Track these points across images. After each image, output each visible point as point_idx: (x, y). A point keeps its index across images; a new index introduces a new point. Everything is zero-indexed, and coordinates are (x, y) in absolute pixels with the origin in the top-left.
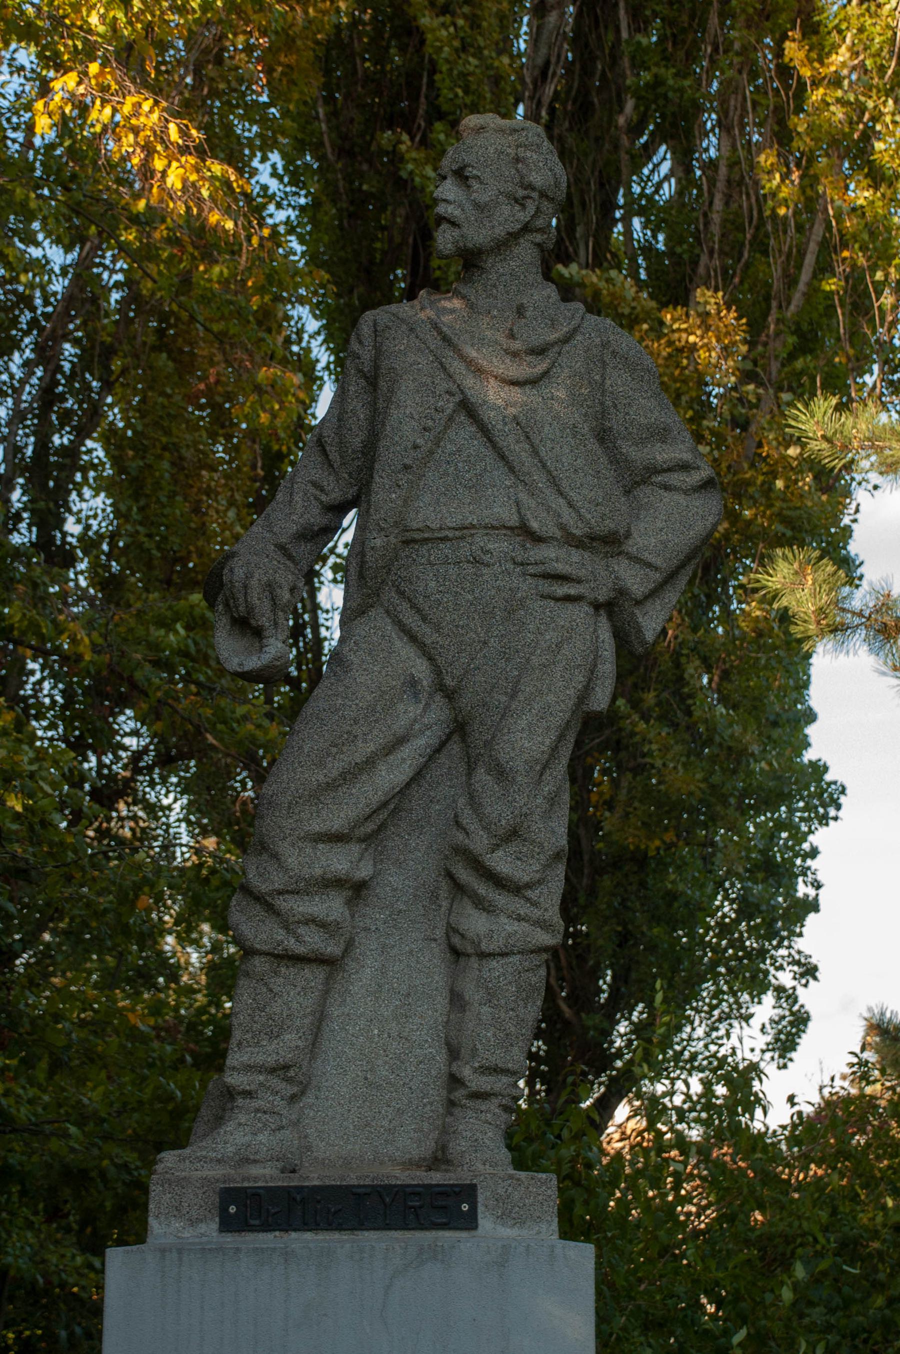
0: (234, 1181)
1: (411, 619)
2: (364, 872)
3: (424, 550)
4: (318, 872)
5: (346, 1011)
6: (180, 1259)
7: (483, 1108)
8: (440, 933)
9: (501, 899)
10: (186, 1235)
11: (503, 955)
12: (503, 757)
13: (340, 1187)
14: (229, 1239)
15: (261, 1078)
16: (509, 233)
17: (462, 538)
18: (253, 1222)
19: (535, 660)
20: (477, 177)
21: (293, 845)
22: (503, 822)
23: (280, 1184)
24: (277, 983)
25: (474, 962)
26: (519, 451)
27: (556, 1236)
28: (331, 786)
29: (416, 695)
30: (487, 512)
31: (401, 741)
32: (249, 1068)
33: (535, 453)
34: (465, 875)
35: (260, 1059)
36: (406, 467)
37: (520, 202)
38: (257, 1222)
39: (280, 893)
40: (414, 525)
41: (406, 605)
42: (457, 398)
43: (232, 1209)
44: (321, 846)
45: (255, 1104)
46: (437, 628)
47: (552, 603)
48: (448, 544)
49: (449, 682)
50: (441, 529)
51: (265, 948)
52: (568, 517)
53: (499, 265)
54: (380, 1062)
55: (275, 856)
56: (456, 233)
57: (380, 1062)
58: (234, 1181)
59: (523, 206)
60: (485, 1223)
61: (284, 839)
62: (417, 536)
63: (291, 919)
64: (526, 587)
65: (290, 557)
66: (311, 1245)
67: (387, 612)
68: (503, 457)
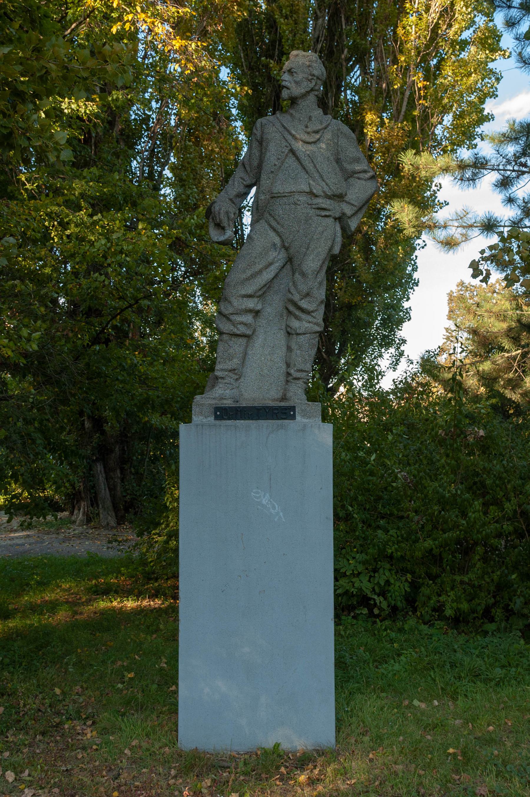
1: (274, 224)
2: (259, 307)
3: (278, 200)
4: (244, 307)
8: (283, 327)
14: (218, 422)
17: (291, 196)
20: (295, 72)
25: (295, 336)
26: (310, 167)
28: (248, 279)
29: (275, 249)
31: (271, 264)
32: (222, 370)
33: (315, 166)
34: (292, 308)
35: (226, 367)
36: (272, 172)
37: (310, 81)
39: (232, 314)
41: (272, 219)
46: (283, 226)
49: (287, 245)
51: (227, 332)
52: (326, 189)
55: (230, 302)
56: (289, 91)
60: (298, 418)
62: (276, 195)
64: (312, 212)
65: (234, 203)
68: (304, 168)
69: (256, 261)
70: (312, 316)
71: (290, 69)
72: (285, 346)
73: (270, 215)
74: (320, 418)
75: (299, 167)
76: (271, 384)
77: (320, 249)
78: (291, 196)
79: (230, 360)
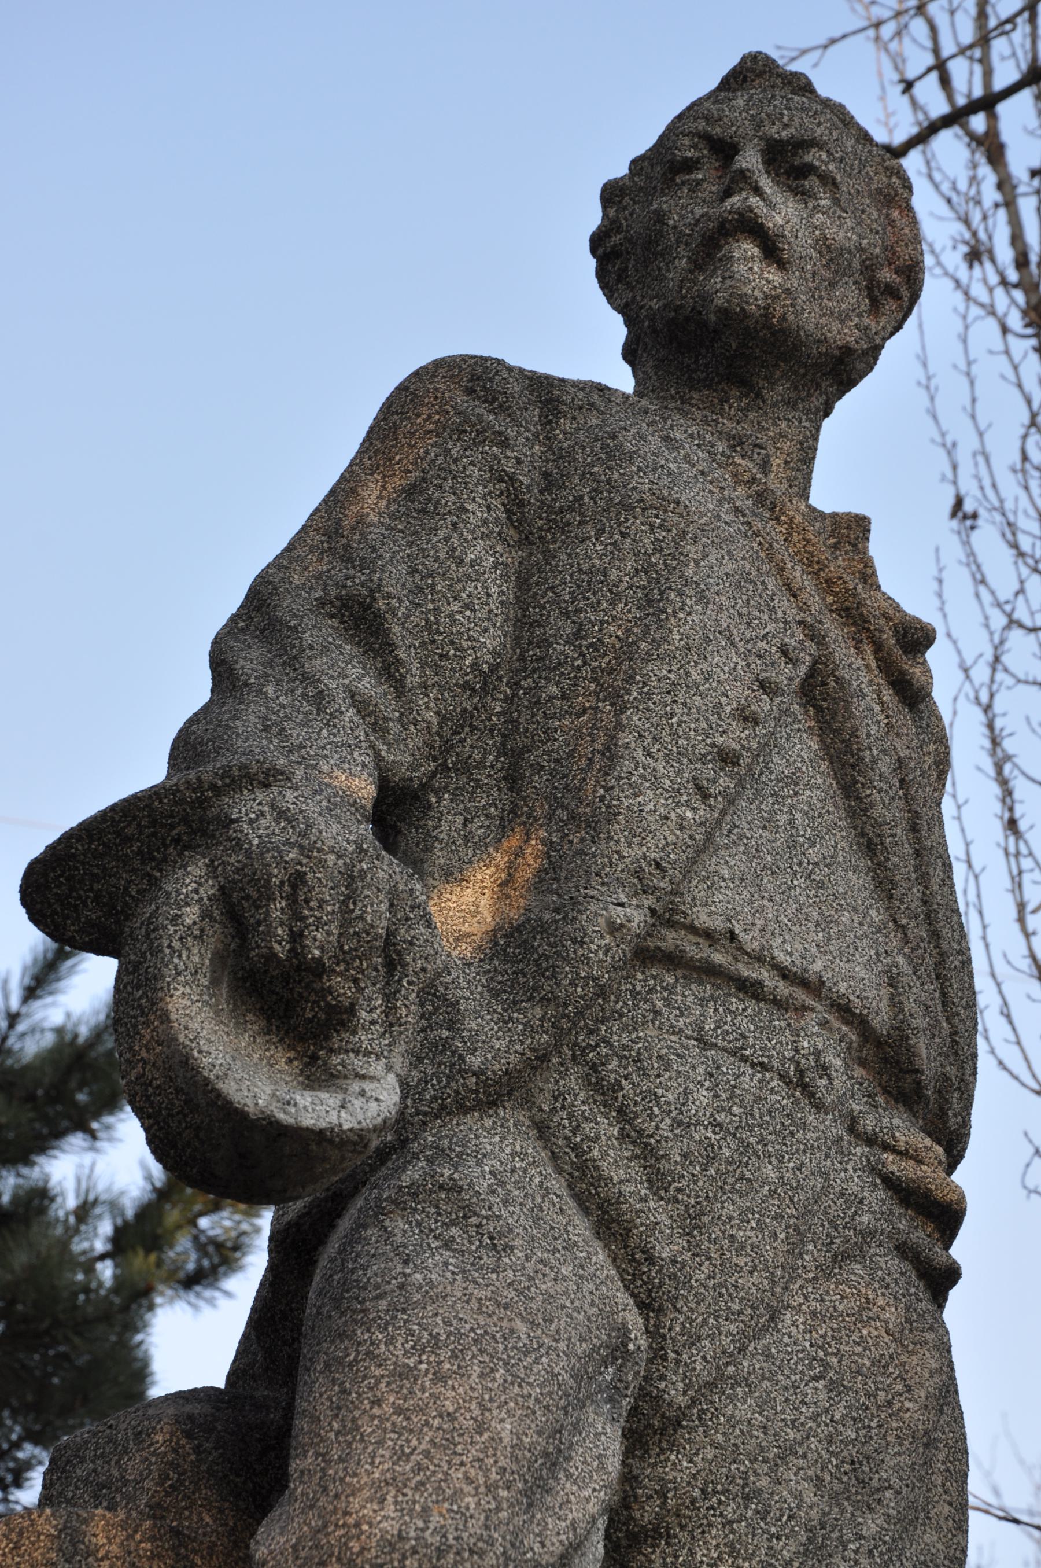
1: (620, 1170)
3: (689, 994)
17: (779, 1004)
20: (828, 181)
40: (702, 918)
41: (608, 1128)
48: (752, 1006)
50: (758, 958)
62: (694, 949)
78: (779, 1004)
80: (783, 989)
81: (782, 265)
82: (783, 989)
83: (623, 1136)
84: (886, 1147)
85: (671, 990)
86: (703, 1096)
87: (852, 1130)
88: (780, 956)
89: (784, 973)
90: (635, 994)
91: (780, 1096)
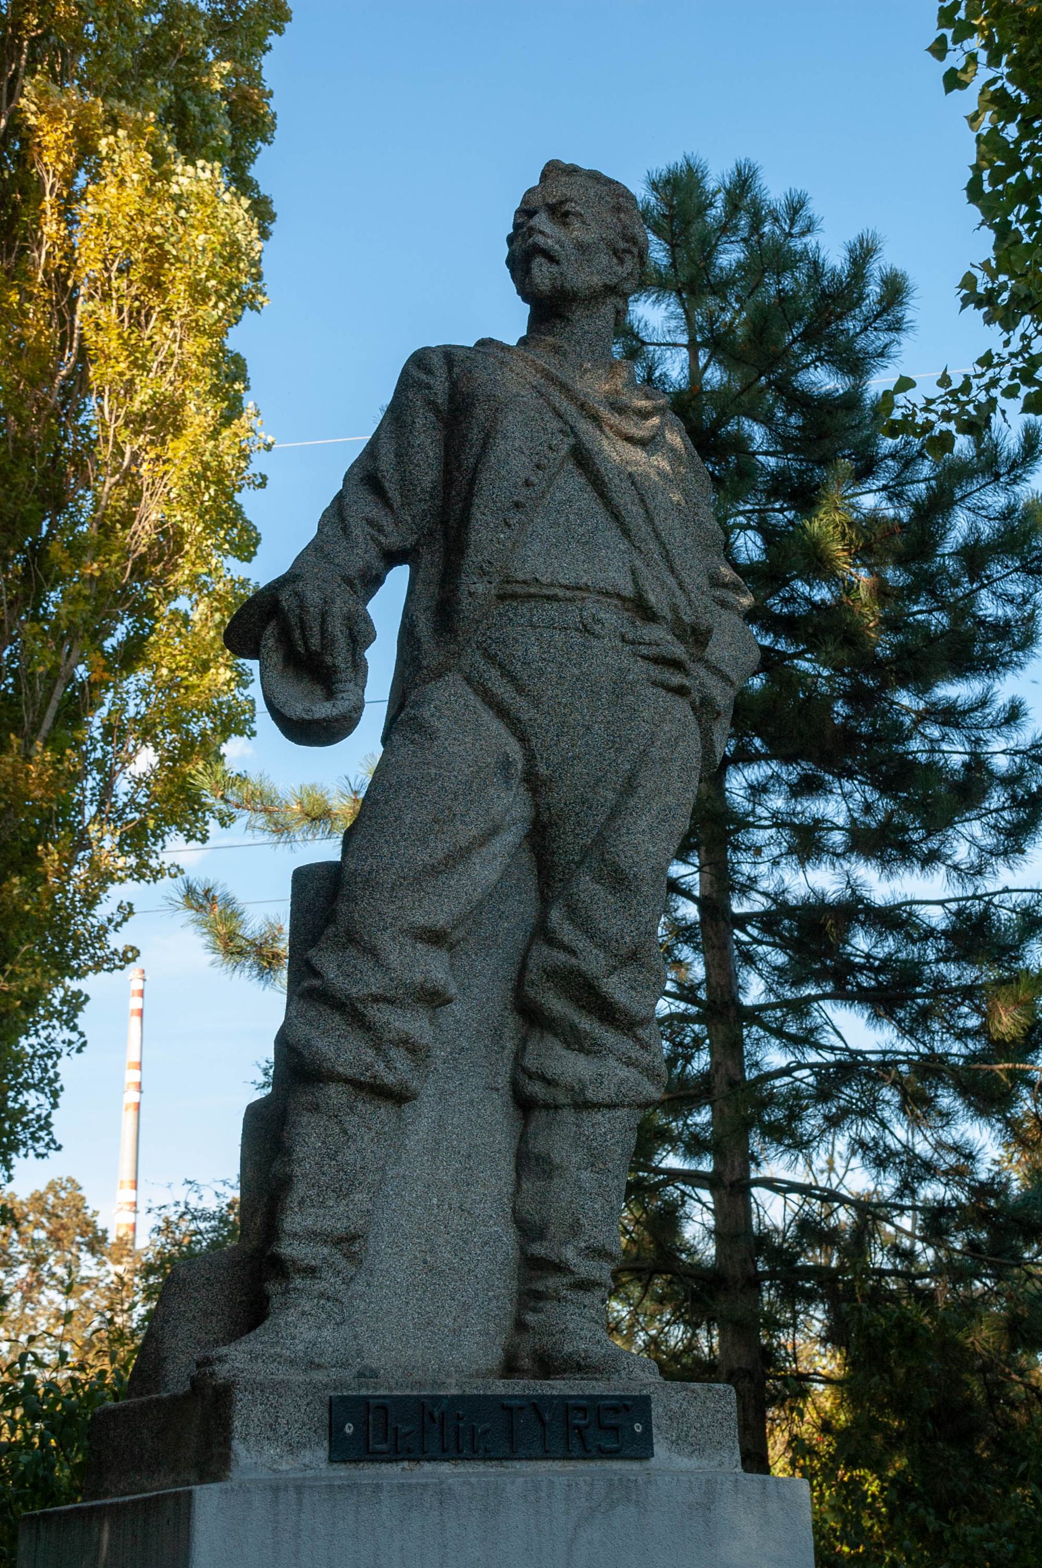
0: (348, 1387)
1: (502, 689)
3: (524, 609)
4: (419, 978)
5: (402, 1171)
6: (300, 1502)
7: (587, 1302)
8: (503, 1081)
9: (609, 1037)
10: (284, 1467)
11: (612, 1106)
12: (624, 863)
13: (485, 1397)
14: (343, 1472)
15: (326, 1251)
16: (605, 286)
17: (571, 600)
18: (379, 1447)
19: (655, 753)
21: (394, 939)
22: (628, 939)
23: (408, 1392)
24: (351, 1121)
25: (568, 1116)
26: (633, 511)
27: (739, 1469)
28: (434, 871)
29: (507, 779)
30: (602, 575)
31: (494, 831)
32: (313, 1236)
33: (650, 519)
34: (557, 1005)
35: (327, 1224)
36: (517, 505)
38: (383, 1447)
39: (376, 999)
40: (520, 576)
41: (495, 673)
42: (572, 441)
43: (349, 1429)
44: (419, 946)
45: (320, 1286)
46: (536, 702)
47: (664, 693)
48: (555, 605)
49: (543, 770)
50: (552, 585)
51: (349, 1072)
52: (681, 600)
53: (584, 321)
54: (441, 1241)
55: (372, 952)
56: (555, 269)
57: (441, 1241)
58: (348, 1387)
59: (622, 262)
60: (660, 1449)
61: (385, 929)
62: (519, 589)
63: (387, 1036)
64: (639, 669)
66: (473, 1480)
67: (468, 680)
69: (459, 809)
70: (638, 1040)
71: (562, 203)
72: (510, 1158)
73: (491, 658)
74: (738, 1456)
75: (598, 508)
76: (465, 1307)
77: (669, 798)
78: (571, 600)
79: (342, 1194)
80: (569, 594)
81: (558, 263)
82: (569, 594)
83: (502, 676)
84: (640, 643)
85: (516, 608)
86: (535, 649)
87: (623, 640)
88: (563, 581)
89: (567, 588)
90: (500, 614)
91: (577, 638)
